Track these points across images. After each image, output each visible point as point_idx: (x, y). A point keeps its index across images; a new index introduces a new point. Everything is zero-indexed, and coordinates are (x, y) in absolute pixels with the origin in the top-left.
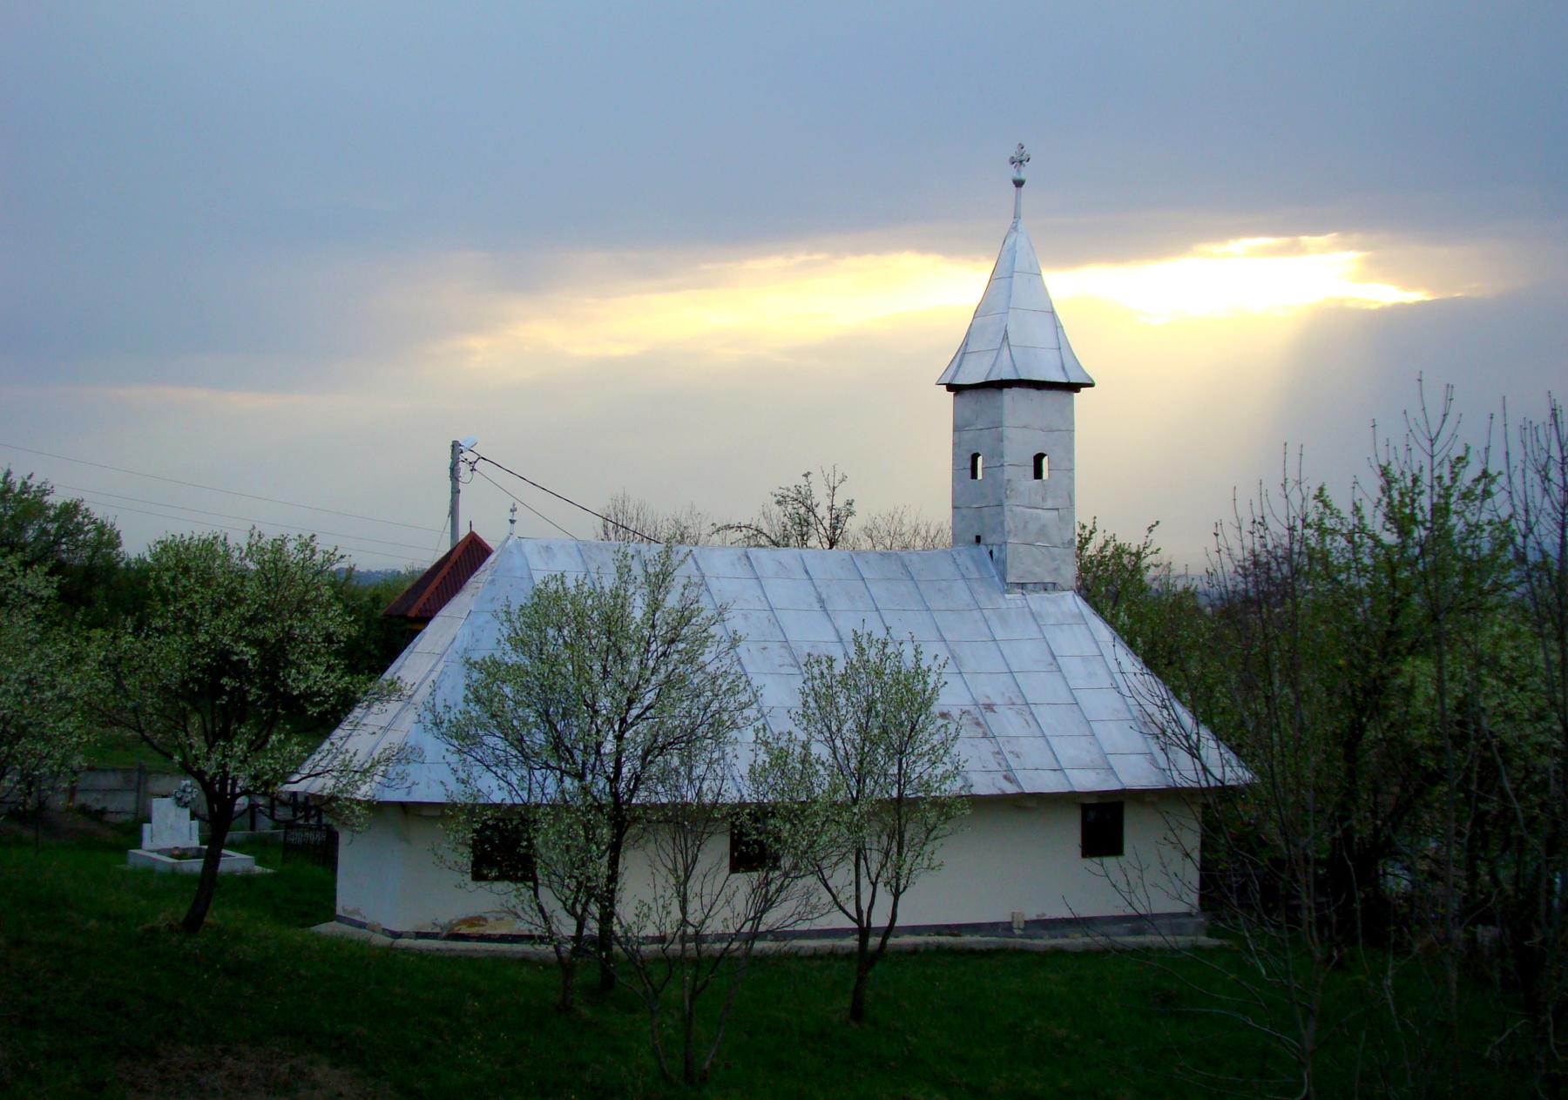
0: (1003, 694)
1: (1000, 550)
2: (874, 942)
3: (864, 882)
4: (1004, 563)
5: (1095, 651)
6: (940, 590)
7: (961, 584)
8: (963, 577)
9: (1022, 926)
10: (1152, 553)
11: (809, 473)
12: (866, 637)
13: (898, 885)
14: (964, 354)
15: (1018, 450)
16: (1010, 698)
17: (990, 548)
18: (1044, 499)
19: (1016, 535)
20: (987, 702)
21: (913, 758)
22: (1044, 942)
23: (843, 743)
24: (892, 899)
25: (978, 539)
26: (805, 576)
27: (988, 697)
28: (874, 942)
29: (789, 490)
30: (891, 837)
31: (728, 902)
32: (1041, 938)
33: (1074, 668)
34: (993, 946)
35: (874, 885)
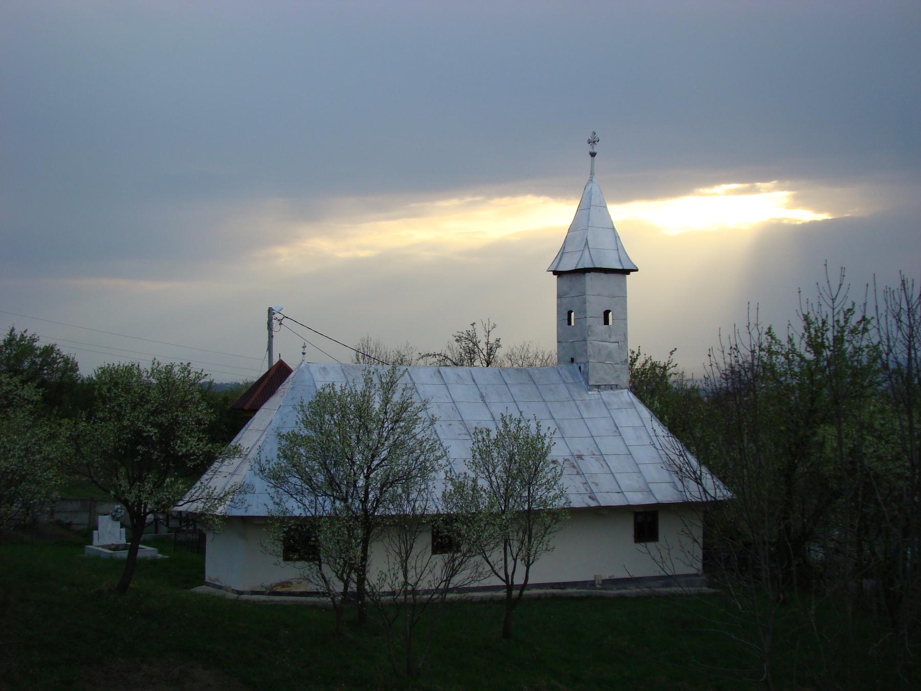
0: (588, 449)
1: (585, 367)
2: (515, 593)
3: (509, 558)
4: (588, 374)
5: (641, 424)
6: (550, 390)
7: (562, 386)
8: (564, 382)
9: (601, 582)
10: (673, 367)
11: (474, 323)
12: (508, 417)
13: (529, 560)
14: (563, 253)
15: (595, 308)
16: (592, 451)
17: (579, 365)
18: (610, 337)
19: (594, 357)
20: (579, 454)
21: (537, 487)
22: (614, 592)
23: (496, 479)
24: (525, 568)
25: (572, 360)
26: (473, 383)
27: (579, 451)
28: (515, 593)
29: (463, 333)
30: (524, 533)
31: (431, 571)
32: (612, 589)
33: (628, 434)
34: (584, 595)
35: (515, 560)
